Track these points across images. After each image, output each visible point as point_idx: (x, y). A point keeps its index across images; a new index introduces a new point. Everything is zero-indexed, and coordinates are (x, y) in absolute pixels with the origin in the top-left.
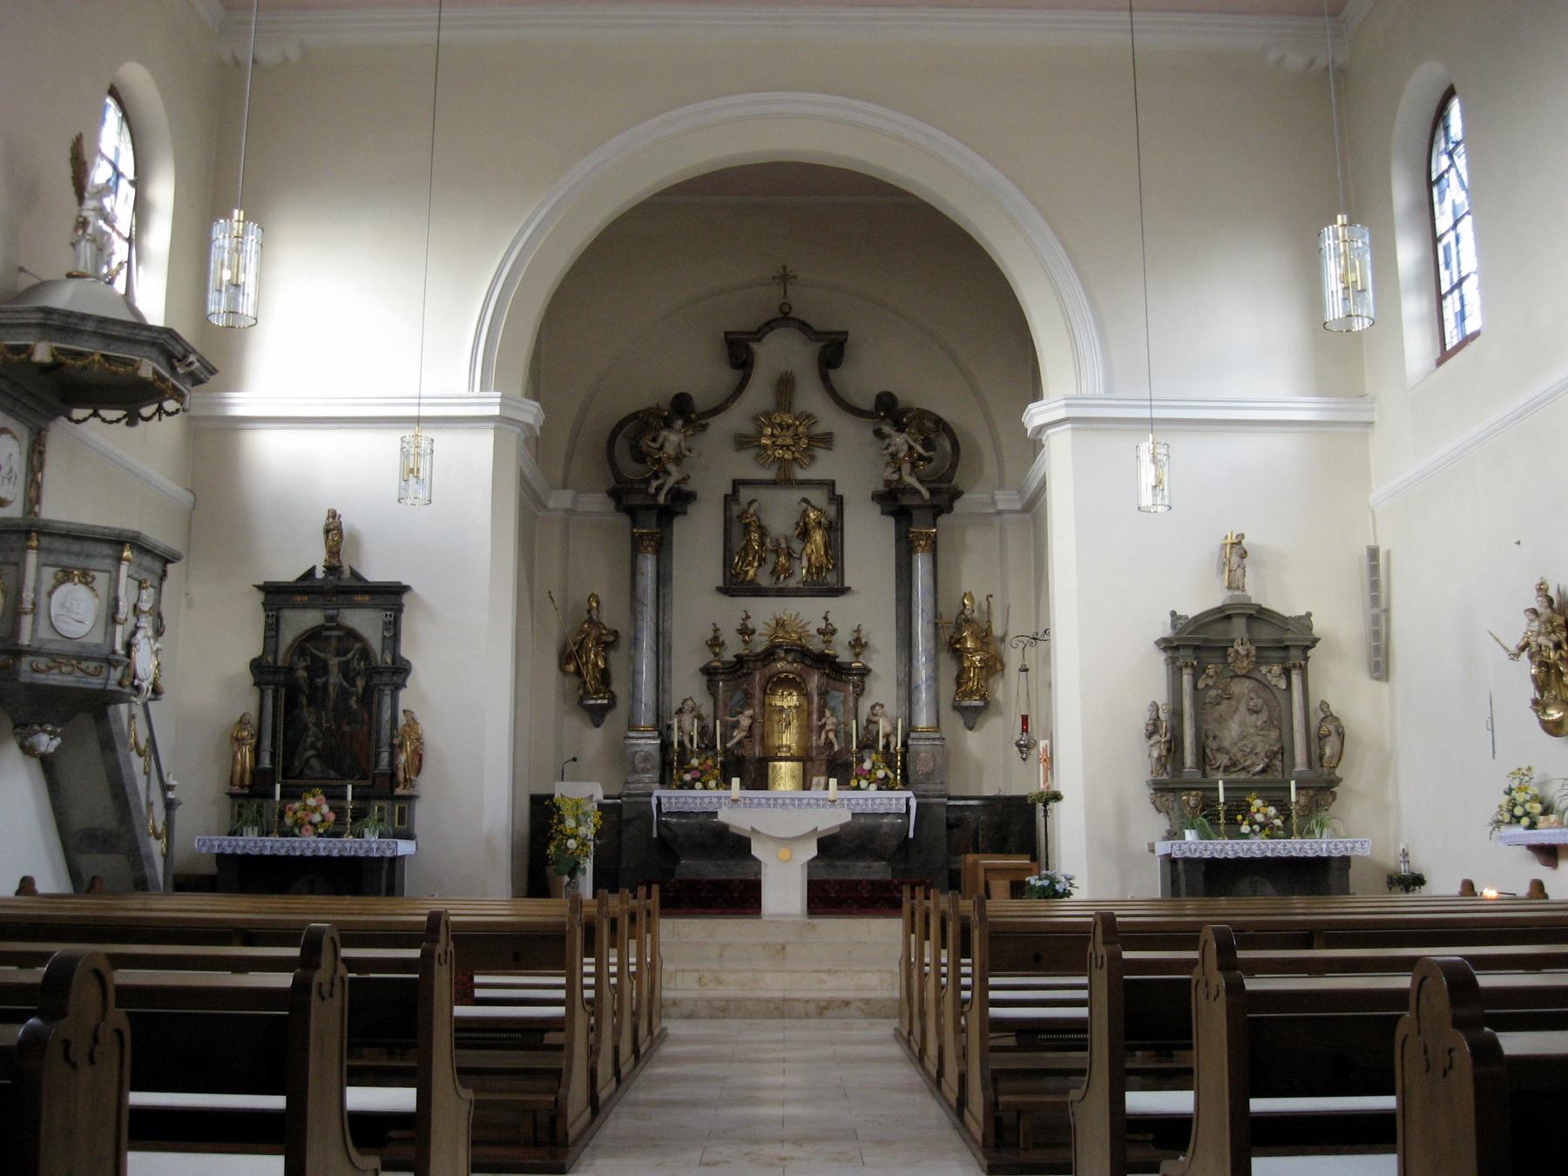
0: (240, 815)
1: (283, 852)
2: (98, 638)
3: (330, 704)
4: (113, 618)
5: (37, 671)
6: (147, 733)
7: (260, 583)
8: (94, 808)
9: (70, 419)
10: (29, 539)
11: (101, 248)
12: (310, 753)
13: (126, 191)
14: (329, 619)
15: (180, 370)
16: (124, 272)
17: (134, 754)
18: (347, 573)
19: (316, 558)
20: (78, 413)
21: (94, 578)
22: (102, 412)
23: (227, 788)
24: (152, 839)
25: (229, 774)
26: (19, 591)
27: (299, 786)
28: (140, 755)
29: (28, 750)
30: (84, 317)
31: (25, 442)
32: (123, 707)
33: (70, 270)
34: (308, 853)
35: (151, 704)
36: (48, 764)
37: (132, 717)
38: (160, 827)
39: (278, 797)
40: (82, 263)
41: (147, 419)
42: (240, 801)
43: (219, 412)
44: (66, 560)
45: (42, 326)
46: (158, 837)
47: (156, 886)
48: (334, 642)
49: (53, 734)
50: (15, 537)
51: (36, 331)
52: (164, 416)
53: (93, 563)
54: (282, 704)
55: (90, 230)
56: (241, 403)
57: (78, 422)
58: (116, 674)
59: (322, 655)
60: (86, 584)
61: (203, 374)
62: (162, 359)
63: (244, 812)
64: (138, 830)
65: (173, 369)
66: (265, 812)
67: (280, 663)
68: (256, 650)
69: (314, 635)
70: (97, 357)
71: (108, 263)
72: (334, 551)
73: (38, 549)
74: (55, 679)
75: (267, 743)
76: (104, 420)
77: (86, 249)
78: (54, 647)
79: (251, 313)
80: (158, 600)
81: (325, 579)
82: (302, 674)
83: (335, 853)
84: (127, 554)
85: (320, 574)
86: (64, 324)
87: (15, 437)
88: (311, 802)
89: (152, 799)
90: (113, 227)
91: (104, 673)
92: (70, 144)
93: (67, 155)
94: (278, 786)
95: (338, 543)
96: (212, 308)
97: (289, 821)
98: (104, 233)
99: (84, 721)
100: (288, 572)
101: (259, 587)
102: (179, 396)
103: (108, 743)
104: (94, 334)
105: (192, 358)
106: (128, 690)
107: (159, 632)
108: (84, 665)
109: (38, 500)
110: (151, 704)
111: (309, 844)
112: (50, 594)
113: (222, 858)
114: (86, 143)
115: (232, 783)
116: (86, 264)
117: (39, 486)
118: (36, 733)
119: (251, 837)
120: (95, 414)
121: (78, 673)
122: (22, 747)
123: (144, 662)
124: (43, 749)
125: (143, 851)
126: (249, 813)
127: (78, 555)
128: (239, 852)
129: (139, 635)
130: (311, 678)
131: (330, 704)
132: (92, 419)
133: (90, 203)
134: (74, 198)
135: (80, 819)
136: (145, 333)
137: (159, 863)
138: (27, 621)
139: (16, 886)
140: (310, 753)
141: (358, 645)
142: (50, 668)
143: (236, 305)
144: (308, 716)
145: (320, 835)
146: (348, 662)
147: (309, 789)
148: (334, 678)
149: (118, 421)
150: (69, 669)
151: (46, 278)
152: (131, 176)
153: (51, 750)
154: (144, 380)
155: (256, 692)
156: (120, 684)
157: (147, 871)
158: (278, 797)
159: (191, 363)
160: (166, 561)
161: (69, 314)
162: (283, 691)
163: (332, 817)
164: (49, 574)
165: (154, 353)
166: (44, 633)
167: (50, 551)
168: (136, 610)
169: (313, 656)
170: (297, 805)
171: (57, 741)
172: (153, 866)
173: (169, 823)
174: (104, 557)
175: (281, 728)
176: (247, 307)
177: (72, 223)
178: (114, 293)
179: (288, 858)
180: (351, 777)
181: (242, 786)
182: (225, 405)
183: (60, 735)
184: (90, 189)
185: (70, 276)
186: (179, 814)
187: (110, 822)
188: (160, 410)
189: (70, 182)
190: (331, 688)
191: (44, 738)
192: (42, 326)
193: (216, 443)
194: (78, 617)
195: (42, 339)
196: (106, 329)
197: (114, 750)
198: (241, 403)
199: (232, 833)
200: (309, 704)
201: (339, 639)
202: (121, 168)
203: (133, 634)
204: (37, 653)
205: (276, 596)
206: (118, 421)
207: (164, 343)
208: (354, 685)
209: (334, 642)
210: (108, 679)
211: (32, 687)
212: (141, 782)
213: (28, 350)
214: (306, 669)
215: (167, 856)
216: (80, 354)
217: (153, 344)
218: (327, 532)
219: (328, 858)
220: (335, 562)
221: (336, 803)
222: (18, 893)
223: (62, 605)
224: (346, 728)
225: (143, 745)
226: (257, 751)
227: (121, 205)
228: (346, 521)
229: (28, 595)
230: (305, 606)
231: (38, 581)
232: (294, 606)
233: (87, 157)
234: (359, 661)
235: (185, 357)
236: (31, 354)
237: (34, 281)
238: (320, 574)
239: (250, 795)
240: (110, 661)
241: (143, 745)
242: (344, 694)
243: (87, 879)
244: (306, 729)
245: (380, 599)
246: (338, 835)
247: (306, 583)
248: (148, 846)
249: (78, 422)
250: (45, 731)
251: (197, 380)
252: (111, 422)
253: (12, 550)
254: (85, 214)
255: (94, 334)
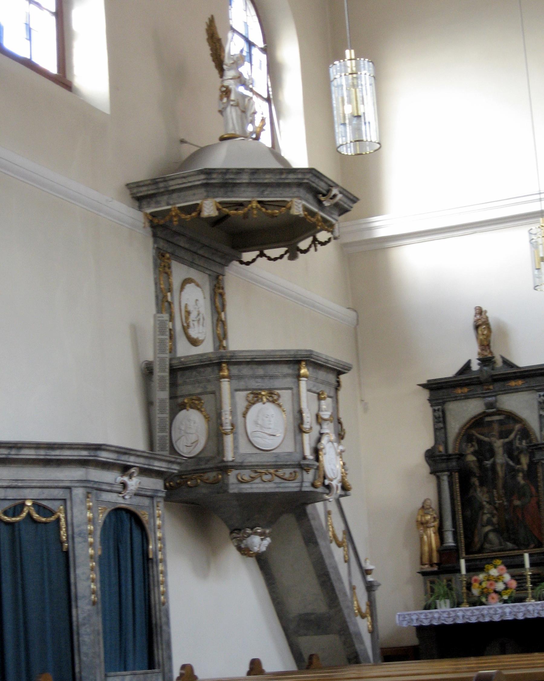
0: (432, 590)
1: (473, 620)
2: (289, 447)
3: (500, 483)
4: (300, 430)
5: (242, 482)
6: (342, 527)
7: (424, 382)
8: (306, 597)
9: (242, 262)
10: (221, 370)
11: (245, 110)
12: (488, 528)
13: (260, 58)
14: (490, 405)
15: (326, 204)
16: (267, 127)
17: (333, 546)
18: (499, 363)
19: (469, 352)
20: (247, 256)
21: (279, 396)
22: (267, 252)
23: (418, 568)
24: (359, 618)
25: (418, 554)
26: (219, 415)
27: (481, 560)
28: (339, 545)
29: (245, 551)
30: (240, 171)
31: (207, 288)
32: (319, 506)
33: (222, 133)
34: (496, 619)
35: (342, 500)
36: (263, 561)
37: (328, 513)
38: (364, 608)
39: (463, 571)
40: (231, 126)
41: (305, 251)
42: (431, 578)
43: (366, 237)
44: (254, 384)
45: (205, 185)
46: (363, 617)
47: (367, 659)
48: (496, 426)
49: (263, 535)
50: (209, 369)
51: (202, 191)
52: (319, 246)
53: (277, 383)
54: (457, 487)
55: (233, 97)
56: (383, 226)
57: (248, 263)
58: (309, 477)
59: (486, 439)
60: (273, 402)
61: (346, 204)
62: (310, 197)
63: (436, 588)
64: (346, 612)
65: (320, 203)
66: (454, 586)
67: (451, 451)
68: (426, 440)
69: (478, 422)
70: (254, 204)
71: (252, 122)
72: (485, 345)
73: (229, 377)
74: (258, 487)
75: (448, 524)
76: (269, 259)
77: (232, 113)
78: (254, 460)
79: (375, 139)
80: (336, 408)
81: (480, 370)
82: (471, 458)
83: (520, 617)
84: (303, 371)
85: (475, 366)
86: (223, 181)
87: (198, 285)
88: (494, 572)
89: (354, 583)
90: (251, 90)
91: (299, 477)
92: (205, 27)
93: (204, 36)
94: (463, 562)
95: (488, 336)
96: (340, 141)
97: (476, 591)
98: (244, 97)
99: (288, 520)
100: (447, 369)
101: (424, 386)
102: (329, 226)
103: (310, 539)
104: (249, 184)
105: (335, 191)
106: (320, 490)
107: (340, 436)
108: (281, 472)
109: (225, 336)
110: (342, 500)
111: (496, 611)
112: (244, 415)
113: (421, 630)
114: (218, 24)
115: (422, 564)
116: (233, 127)
117: (224, 323)
118: (249, 535)
119: (444, 609)
120: (262, 255)
121: (277, 480)
122: (239, 549)
123: (332, 464)
124: (256, 549)
125: (352, 629)
126: (441, 588)
127: (262, 377)
128: (435, 623)
129: (324, 441)
130: (480, 461)
131: (500, 483)
132: (259, 259)
133: (229, 74)
134: (216, 72)
135: (296, 607)
136: (291, 176)
137: (367, 639)
138: (229, 440)
139: (247, 668)
140: (488, 528)
141: (518, 427)
142: (253, 478)
143: (360, 134)
144: (481, 495)
145: (505, 602)
146: (511, 443)
147: (490, 560)
148: (501, 458)
149: (281, 257)
150: (268, 477)
151: (202, 146)
152: (262, 45)
153: (264, 549)
154: (297, 217)
155: (433, 478)
156: (313, 485)
157: (357, 646)
158: (463, 571)
159: (335, 196)
160: (339, 373)
161: (226, 171)
162: (456, 475)
163: (514, 584)
164: (241, 396)
165: (302, 192)
166: (244, 448)
167: (240, 378)
168: (319, 419)
169: (480, 442)
170: (481, 576)
171: (267, 541)
172: (362, 642)
173: (371, 603)
174: (285, 376)
175: (459, 508)
176: (370, 133)
177: (217, 93)
178: (263, 146)
179: (479, 624)
180: (527, 547)
181: (431, 565)
182: (371, 229)
183: (269, 535)
184: (227, 61)
185: (222, 139)
186: (379, 594)
187: (320, 607)
188: (315, 240)
189: (210, 59)
190: (499, 469)
191: (256, 539)
192: (205, 185)
193: (368, 263)
194: (270, 432)
195: (207, 197)
196: (258, 178)
197: (316, 543)
198: (383, 226)
199: (427, 607)
200: (482, 484)
201: (501, 422)
202: (251, 39)
203: (319, 440)
204: (241, 466)
205: (440, 391)
206: (281, 257)
207: (310, 182)
208: (518, 462)
209: (496, 426)
210: (302, 482)
211: (240, 496)
212: (343, 569)
213: (196, 208)
214: (474, 453)
215: (373, 632)
216: (241, 205)
217: (299, 185)
218: (477, 327)
219: (515, 622)
220: (487, 354)
221: (517, 571)
222: (249, 673)
223: (256, 423)
224: (517, 503)
225: (340, 536)
226: (440, 532)
227: (256, 71)
228: (492, 315)
229: (227, 418)
230: (466, 397)
231: (234, 405)
232: (456, 399)
233: (220, 35)
234: (521, 440)
235: (329, 191)
236: (200, 212)
237: (194, 149)
238: (475, 366)
239: (439, 571)
240: (302, 467)
241: (340, 536)
242: (512, 472)
243: (306, 657)
244: (482, 507)
245: (532, 382)
246: (521, 600)
247: (463, 377)
248: (356, 625)
249: (248, 263)
250: (256, 533)
251: (343, 210)
252: (275, 259)
253: (209, 381)
254: (226, 83)
255: (249, 184)
